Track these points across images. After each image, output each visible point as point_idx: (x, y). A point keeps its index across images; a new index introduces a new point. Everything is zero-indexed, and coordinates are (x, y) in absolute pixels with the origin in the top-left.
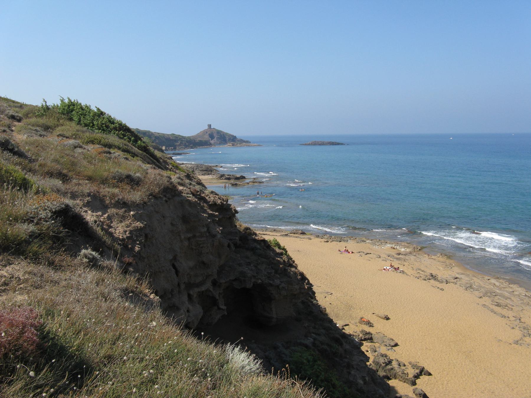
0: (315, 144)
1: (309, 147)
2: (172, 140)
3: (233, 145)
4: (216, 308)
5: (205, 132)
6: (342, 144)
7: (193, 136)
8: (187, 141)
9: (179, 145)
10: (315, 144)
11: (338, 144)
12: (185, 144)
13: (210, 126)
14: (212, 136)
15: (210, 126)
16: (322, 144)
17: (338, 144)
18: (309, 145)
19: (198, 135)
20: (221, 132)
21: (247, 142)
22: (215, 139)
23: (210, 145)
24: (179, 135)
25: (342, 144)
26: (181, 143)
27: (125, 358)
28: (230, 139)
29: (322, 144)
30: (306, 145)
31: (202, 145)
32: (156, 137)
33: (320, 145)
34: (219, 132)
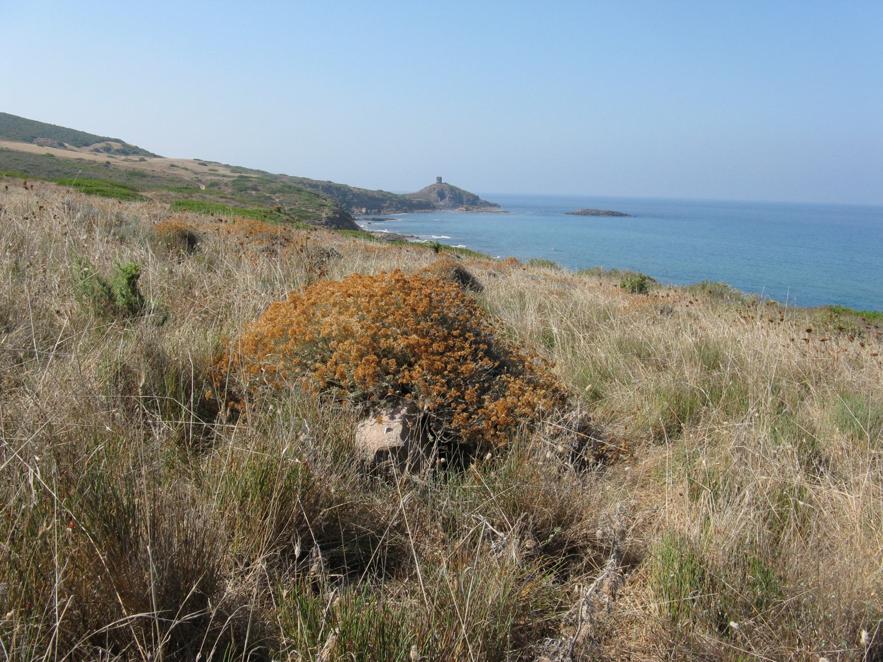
0: (586, 213)
1: (572, 217)
2: (377, 199)
3: (467, 210)
4: (23, 181)
5: (431, 189)
6: (626, 215)
7: (410, 195)
8: (400, 202)
9: (388, 207)
10: (586, 213)
11: (621, 215)
12: (397, 205)
13: (439, 179)
14: (441, 195)
15: (439, 179)
16: (597, 214)
17: (621, 215)
18: (578, 214)
19: (420, 194)
20: (457, 189)
21: (495, 205)
22: (447, 199)
23: (434, 208)
24: (389, 193)
25: (626, 215)
26: (390, 204)
27: (271, 407)
28: (468, 200)
29: (597, 214)
30: (573, 214)
31: (421, 209)
32: (353, 195)
33: (593, 215)
34: (453, 189)
